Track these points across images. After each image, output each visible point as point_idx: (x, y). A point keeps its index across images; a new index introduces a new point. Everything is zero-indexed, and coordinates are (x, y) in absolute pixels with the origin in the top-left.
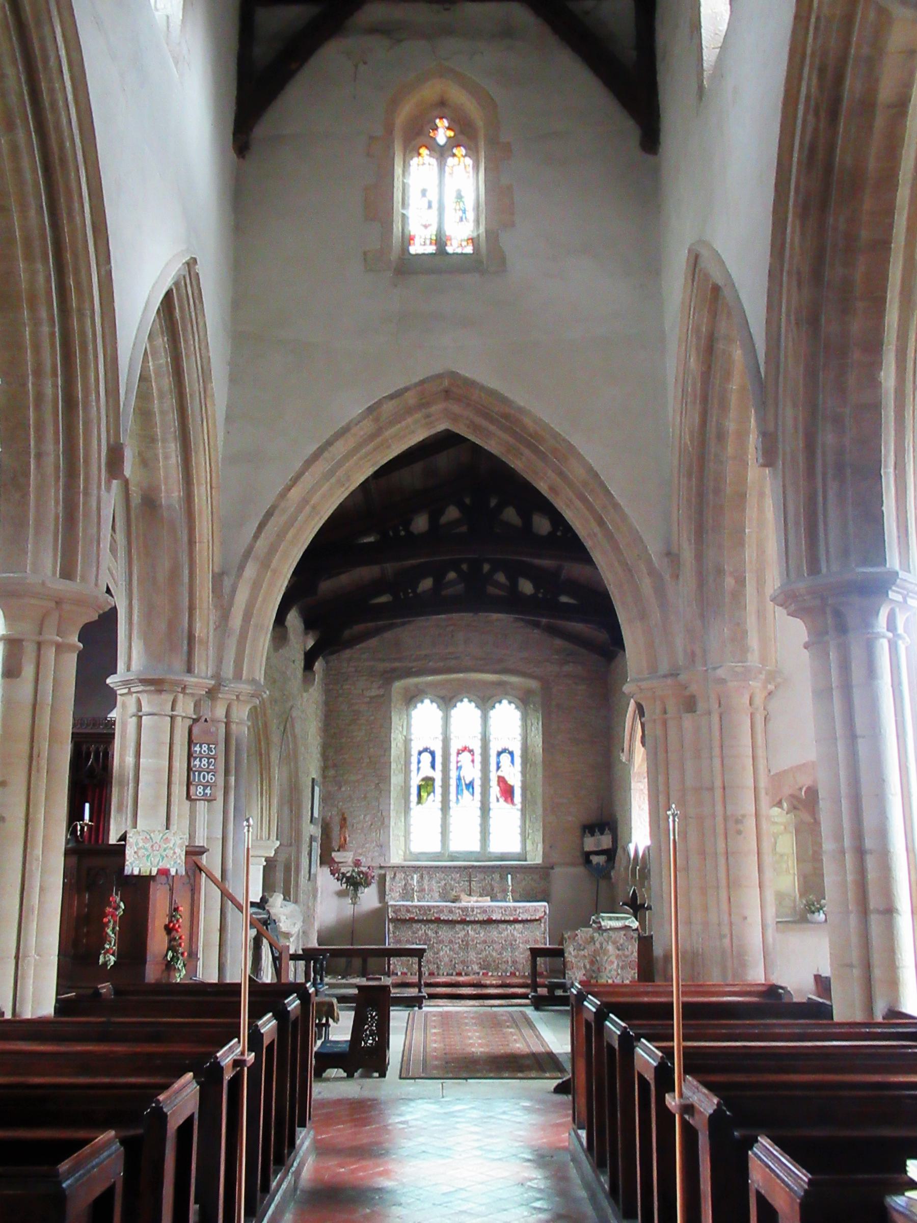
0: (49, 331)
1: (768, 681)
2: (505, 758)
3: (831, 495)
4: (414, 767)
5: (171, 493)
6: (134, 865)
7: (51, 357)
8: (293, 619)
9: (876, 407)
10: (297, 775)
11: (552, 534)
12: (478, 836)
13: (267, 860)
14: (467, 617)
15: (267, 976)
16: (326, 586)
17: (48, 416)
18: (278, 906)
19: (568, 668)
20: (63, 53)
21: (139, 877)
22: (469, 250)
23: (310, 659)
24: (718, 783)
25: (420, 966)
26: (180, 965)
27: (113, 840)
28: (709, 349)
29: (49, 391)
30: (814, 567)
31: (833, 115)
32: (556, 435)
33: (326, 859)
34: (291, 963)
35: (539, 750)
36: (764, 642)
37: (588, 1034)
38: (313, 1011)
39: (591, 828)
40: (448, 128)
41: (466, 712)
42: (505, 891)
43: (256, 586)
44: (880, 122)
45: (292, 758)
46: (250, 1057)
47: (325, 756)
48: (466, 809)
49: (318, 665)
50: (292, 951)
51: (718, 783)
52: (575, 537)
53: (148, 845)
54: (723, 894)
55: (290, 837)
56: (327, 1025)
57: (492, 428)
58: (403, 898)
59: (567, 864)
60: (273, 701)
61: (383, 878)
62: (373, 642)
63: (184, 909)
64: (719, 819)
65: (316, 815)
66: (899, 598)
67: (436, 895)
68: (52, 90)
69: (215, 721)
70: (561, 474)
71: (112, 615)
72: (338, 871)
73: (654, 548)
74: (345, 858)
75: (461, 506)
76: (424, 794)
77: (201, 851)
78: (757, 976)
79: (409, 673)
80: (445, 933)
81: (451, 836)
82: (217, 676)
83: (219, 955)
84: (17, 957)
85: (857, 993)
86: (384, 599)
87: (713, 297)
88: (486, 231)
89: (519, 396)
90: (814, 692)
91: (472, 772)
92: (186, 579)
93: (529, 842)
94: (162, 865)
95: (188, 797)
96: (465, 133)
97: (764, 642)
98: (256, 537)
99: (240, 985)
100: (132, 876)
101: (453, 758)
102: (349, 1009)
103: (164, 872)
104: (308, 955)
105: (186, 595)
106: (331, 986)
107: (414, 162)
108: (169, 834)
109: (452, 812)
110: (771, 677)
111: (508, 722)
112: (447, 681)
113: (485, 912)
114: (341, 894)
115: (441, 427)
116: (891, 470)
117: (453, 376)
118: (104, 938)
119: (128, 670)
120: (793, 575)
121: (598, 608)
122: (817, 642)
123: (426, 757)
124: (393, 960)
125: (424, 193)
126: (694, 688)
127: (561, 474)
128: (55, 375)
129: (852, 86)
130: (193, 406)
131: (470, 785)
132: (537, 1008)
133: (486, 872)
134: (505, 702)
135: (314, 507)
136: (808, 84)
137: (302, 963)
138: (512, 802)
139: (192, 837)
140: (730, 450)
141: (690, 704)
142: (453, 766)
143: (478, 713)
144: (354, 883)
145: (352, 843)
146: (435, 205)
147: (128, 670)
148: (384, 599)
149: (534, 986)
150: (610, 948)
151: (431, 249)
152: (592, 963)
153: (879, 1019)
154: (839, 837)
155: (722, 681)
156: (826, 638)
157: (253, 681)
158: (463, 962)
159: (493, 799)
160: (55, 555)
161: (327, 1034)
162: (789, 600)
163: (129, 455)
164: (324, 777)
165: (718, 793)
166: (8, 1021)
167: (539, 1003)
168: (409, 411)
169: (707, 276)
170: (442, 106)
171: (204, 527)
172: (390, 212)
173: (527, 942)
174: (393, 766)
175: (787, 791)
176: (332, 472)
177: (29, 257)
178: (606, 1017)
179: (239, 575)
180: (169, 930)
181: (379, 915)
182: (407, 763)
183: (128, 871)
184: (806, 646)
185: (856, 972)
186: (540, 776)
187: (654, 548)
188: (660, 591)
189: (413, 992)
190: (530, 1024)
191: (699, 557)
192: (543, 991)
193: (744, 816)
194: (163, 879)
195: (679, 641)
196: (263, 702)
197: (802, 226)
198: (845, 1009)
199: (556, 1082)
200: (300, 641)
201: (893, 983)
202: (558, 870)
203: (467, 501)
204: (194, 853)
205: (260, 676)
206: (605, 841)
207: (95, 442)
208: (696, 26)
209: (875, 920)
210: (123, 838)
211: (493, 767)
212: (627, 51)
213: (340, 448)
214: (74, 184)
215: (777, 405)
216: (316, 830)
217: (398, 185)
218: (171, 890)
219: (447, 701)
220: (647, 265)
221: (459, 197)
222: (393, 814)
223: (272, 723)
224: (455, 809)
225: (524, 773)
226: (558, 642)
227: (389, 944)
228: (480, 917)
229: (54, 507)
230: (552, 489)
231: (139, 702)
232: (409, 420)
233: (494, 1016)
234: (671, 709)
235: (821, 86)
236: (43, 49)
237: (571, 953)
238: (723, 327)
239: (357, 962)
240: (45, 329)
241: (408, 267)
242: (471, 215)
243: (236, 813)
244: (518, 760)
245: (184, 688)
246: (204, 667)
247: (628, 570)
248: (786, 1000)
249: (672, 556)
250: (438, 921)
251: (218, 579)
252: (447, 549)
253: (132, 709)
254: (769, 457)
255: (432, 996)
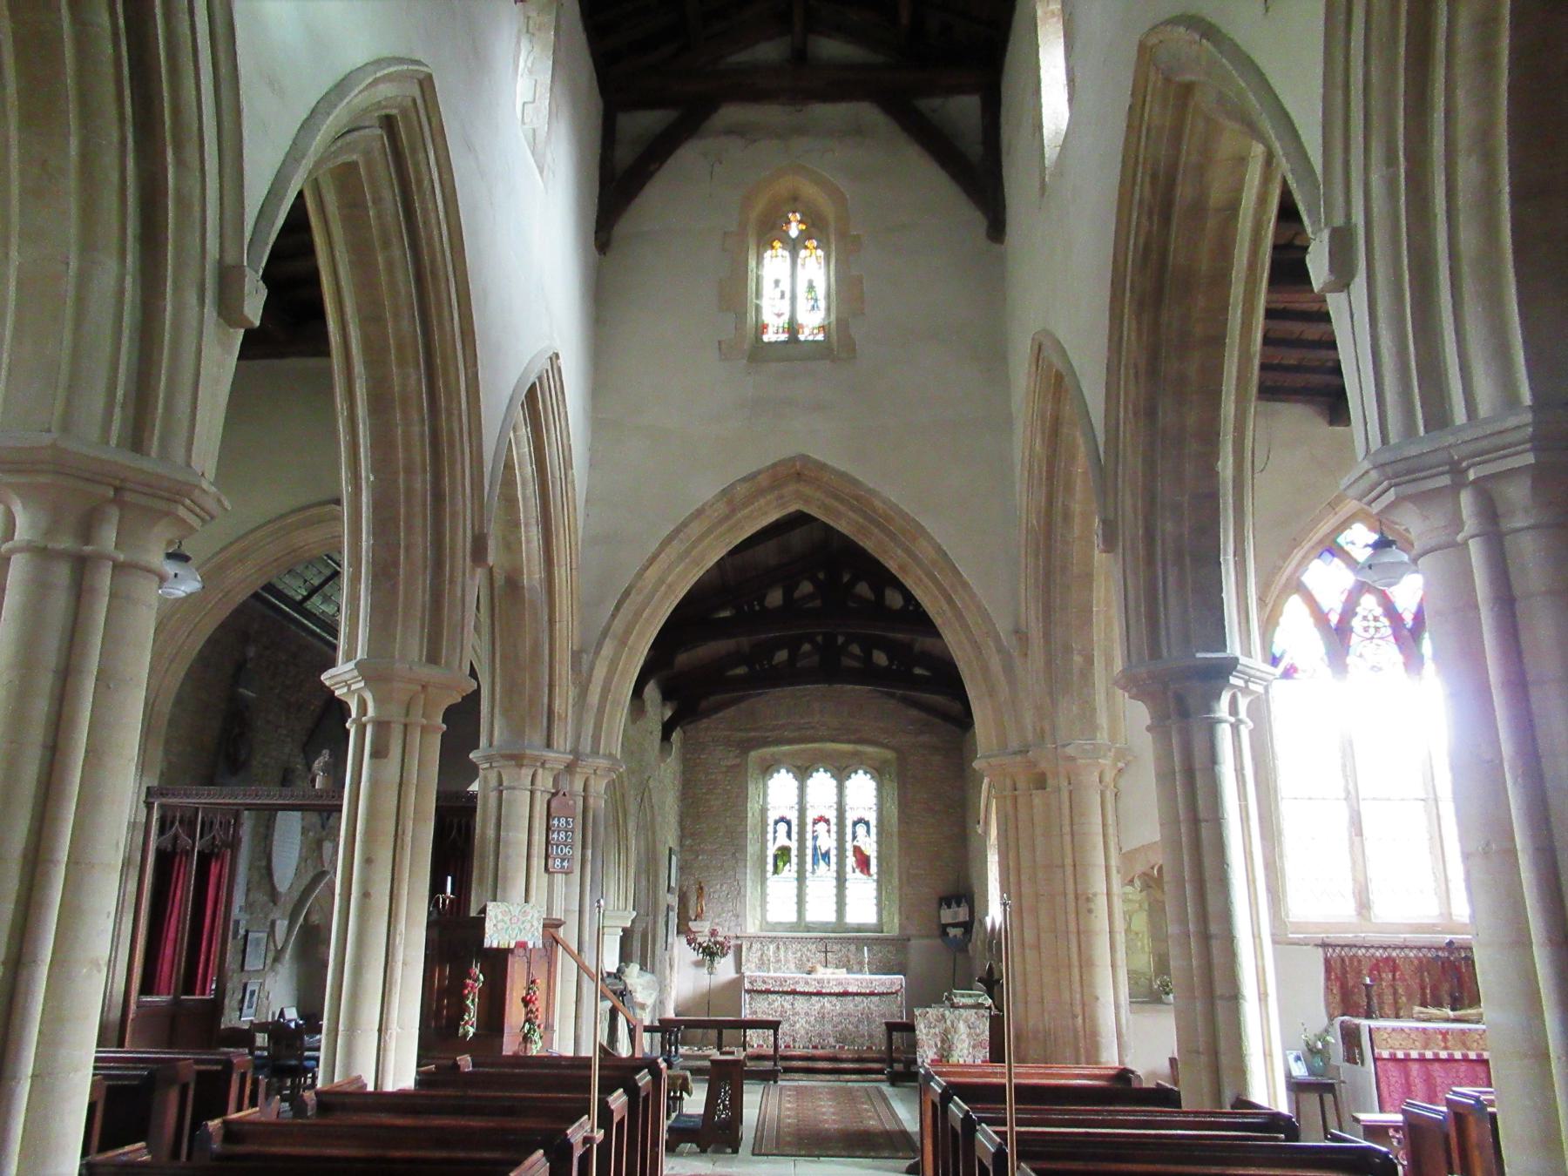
0: (420, 430)
1: (1117, 759)
2: (861, 829)
3: (1171, 579)
4: (770, 836)
5: (532, 575)
6: (493, 938)
7: (421, 454)
8: (652, 691)
9: (1213, 497)
10: (654, 846)
11: (904, 609)
12: (834, 907)
13: (624, 930)
14: (822, 687)
15: (624, 1050)
16: (683, 659)
17: (418, 509)
18: (635, 978)
19: (924, 738)
20: (436, 176)
21: (498, 950)
22: (820, 337)
23: (667, 729)
24: (1069, 861)
25: (776, 1039)
26: (536, 1037)
27: (473, 913)
28: (1054, 433)
29: (418, 486)
30: (1155, 653)
31: (1166, 219)
32: (904, 516)
33: (683, 929)
34: (646, 1036)
35: (895, 820)
36: (1113, 720)
37: (937, 1113)
38: (664, 1086)
39: (947, 900)
40: (800, 222)
41: (822, 784)
42: (861, 963)
43: (613, 664)
44: (1212, 223)
45: (648, 829)
46: (599, 1135)
47: (681, 823)
48: (822, 883)
49: (676, 736)
50: (647, 1023)
51: (1069, 861)
52: (925, 614)
53: (507, 919)
54: (1076, 971)
55: (646, 905)
56: (681, 1098)
57: (842, 508)
58: (759, 968)
59: (922, 937)
60: (631, 772)
61: (739, 948)
62: (730, 712)
63: (541, 982)
64: (1071, 896)
65: (673, 884)
66: (1241, 683)
67: (792, 966)
68: (425, 211)
69: (573, 795)
70: (908, 551)
71: (473, 698)
72: (694, 940)
73: (1003, 627)
74: (702, 929)
75: (814, 580)
76: (780, 864)
77: (558, 924)
78: (1110, 1059)
79: (765, 743)
80: (801, 1003)
81: (808, 906)
82: (575, 752)
83: (567, 1029)
84: (380, 1030)
85: (1205, 1082)
86: (741, 670)
87: (1058, 384)
88: (838, 320)
89: (867, 476)
90: (1157, 775)
91: (827, 842)
92: (547, 658)
93: (885, 913)
94: (519, 939)
95: (546, 869)
96: (816, 228)
97: (1113, 720)
98: (613, 616)
99: (589, 1059)
100: (491, 949)
101: (809, 828)
102: (702, 1081)
103: (522, 945)
104: (665, 1028)
105: (546, 671)
106: (686, 1057)
107: (768, 254)
108: (528, 907)
109: (808, 882)
110: (1121, 754)
111: (863, 791)
112: (804, 751)
113: (840, 984)
114: (698, 964)
115: (792, 508)
116: (1231, 557)
117: (805, 458)
118: (465, 1009)
119: (491, 745)
120: (1134, 658)
121: (947, 679)
122: (1159, 726)
123: (782, 827)
124: (749, 1032)
125: (777, 283)
126: (1044, 766)
127: (908, 551)
128: (424, 471)
129: (1184, 192)
130: (555, 492)
131: (826, 855)
132: (893, 1084)
133: (840, 940)
134: (861, 772)
135: (670, 586)
136: (1142, 190)
137: (658, 1036)
138: (869, 874)
139: (550, 909)
140: (1077, 531)
141: (1040, 782)
142: (809, 836)
143: (834, 783)
144: (710, 953)
145: (709, 913)
146: (788, 295)
147: (491, 745)
148: (741, 670)
149: (891, 1061)
150: (962, 1026)
151: (783, 337)
152: (943, 1041)
153: (1228, 1109)
154: (1183, 921)
155: (1072, 759)
156: (1168, 722)
157: (610, 756)
158: (820, 1035)
159: (849, 869)
160: (422, 638)
161: (681, 1108)
162: (1135, 684)
163: (492, 544)
164: (681, 845)
165: (1069, 870)
166: (370, 1094)
167: (895, 1079)
168: (761, 492)
169: (1050, 365)
170: (795, 202)
171: (563, 604)
172: (744, 304)
173: (883, 1015)
174: (750, 835)
175: (1140, 868)
176: (687, 552)
177: (402, 363)
178: (951, 1099)
179: (597, 653)
180: (526, 1002)
181: (735, 986)
182: (764, 833)
183: (487, 944)
184: (1149, 729)
185: (1204, 1059)
186: (896, 847)
187: (1003, 627)
188: (1009, 669)
189: (768, 1065)
190: (885, 1099)
191: (1047, 636)
192: (898, 1067)
193: (1095, 895)
194: (521, 951)
195: (1028, 718)
196: (620, 776)
197: (1139, 323)
198: (1193, 1099)
199: (907, 1163)
200: (657, 710)
201: (1241, 1071)
202: (913, 942)
203: (821, 576)
204: (551, 926)
205: (617, 751)
206: (962, 914)
207: (460, 532)
208: (1039, 126)
209: (1221, 1006)
210: (483, 910)
211: (849, 837)
212: (973, 148)
213: (696, 529)
214: (445, 296)
215: (1116, 495)
216: (673, 900)
217: (752, 276)
218: (529, 963)
219: (803, 773)
220: (991, 353)
221: (811, 287)
222: (749, 883)
223: (629, 795)
224: (811, 882)
225: (879, 843)
226: (914, 713)
227: (746, 1014)
228: (836, 989)
229: (422, 596)
230: (902, 568)
231: (500, 775)
232: (762, 501)
233: (850, 1091)
234: (1021, 785)
235: (1154, 193)
236: (418, 172)
237: (922, 1031)
238: (1067, 410)
239: (713, 1033)
240: (416, 429)
241: (760, 353)
242: (822, 304)
243: (590, 886)
244: (873, 830)
245: (543, 764)
246: (562, 741)
247: (977, 647)
248: (1135, 1084)
249: (1020, 635)
250: (794, 993)
251: (576, 656)
252: (798, 628)
253: (493, 782)
254: (1110, 543)
255: (787, 1070)
